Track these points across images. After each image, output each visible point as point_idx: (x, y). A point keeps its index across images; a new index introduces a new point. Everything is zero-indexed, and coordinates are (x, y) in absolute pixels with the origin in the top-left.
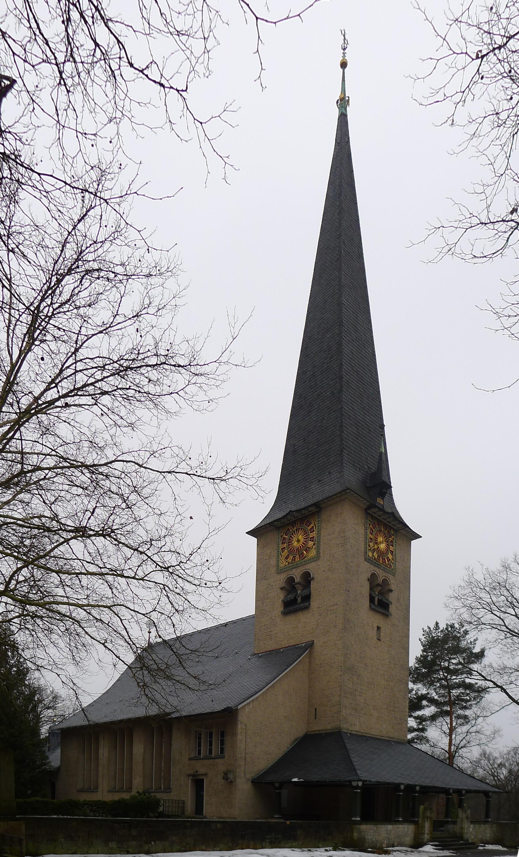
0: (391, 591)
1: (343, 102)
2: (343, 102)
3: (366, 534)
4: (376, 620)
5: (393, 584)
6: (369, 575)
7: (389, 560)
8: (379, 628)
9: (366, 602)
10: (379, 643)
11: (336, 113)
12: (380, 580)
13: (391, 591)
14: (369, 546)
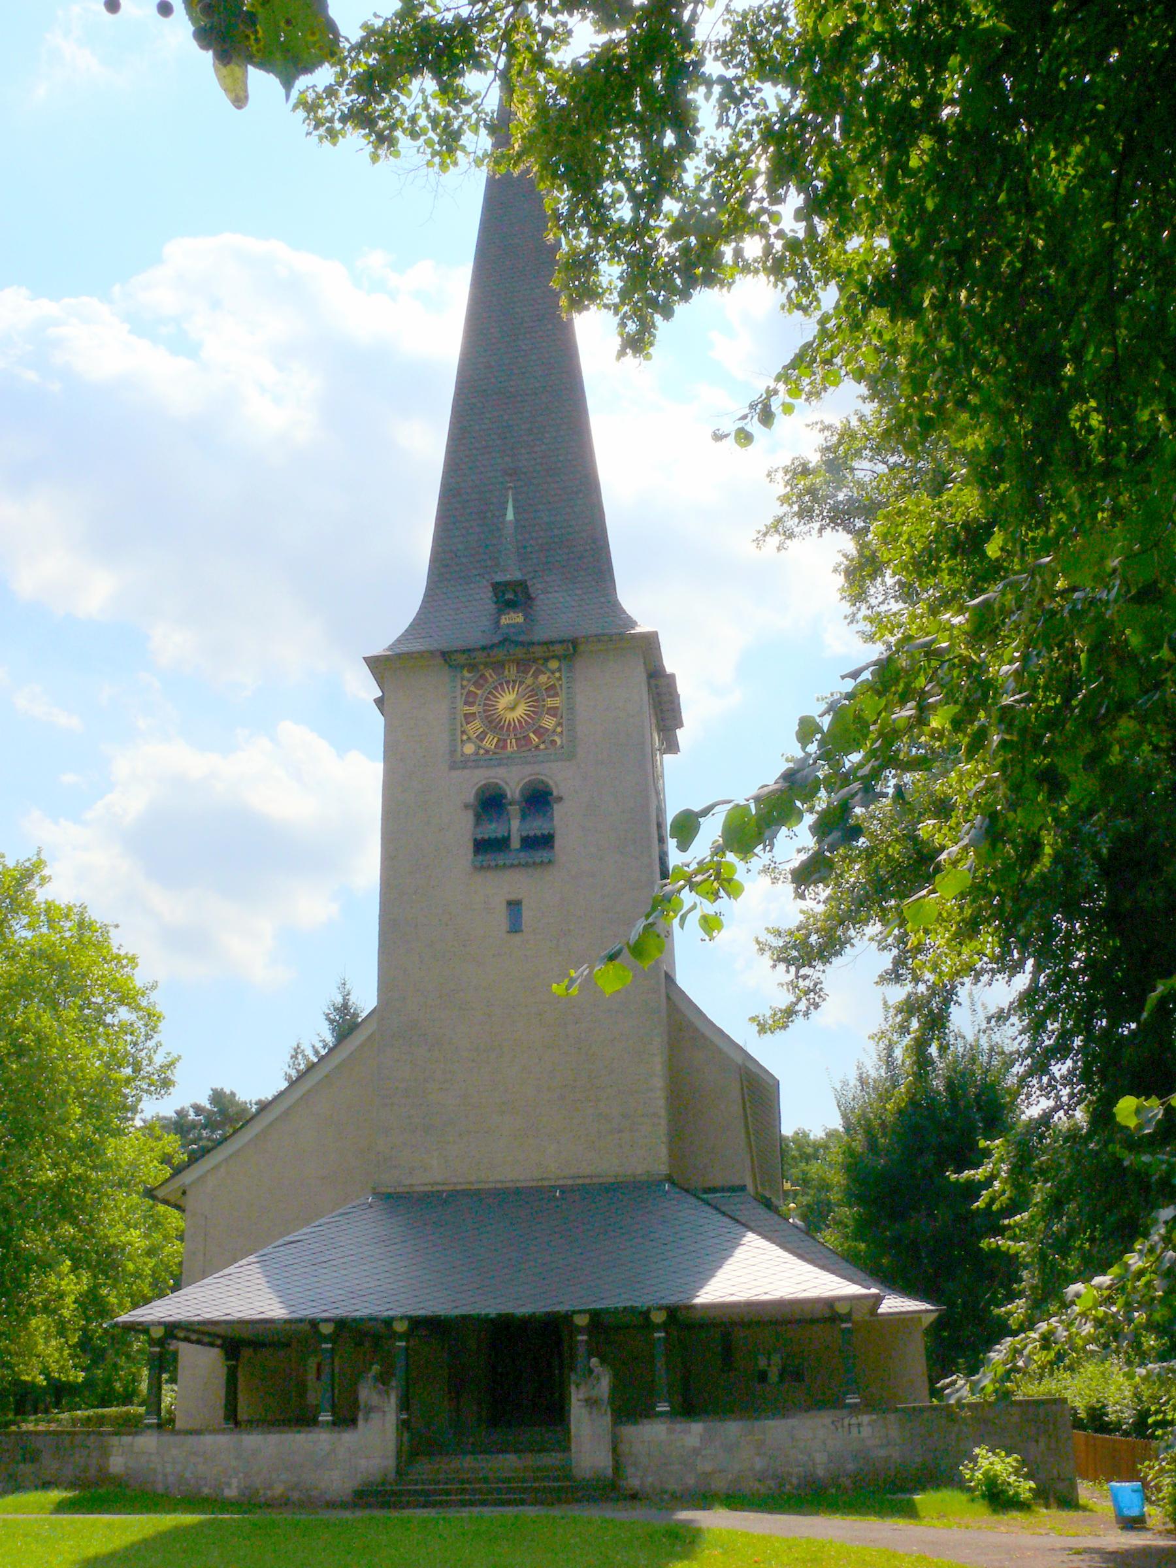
0: (560, 799)
6: (470, 797)
8: (514, 906)
12: (513, 789)
14: (463, 732)
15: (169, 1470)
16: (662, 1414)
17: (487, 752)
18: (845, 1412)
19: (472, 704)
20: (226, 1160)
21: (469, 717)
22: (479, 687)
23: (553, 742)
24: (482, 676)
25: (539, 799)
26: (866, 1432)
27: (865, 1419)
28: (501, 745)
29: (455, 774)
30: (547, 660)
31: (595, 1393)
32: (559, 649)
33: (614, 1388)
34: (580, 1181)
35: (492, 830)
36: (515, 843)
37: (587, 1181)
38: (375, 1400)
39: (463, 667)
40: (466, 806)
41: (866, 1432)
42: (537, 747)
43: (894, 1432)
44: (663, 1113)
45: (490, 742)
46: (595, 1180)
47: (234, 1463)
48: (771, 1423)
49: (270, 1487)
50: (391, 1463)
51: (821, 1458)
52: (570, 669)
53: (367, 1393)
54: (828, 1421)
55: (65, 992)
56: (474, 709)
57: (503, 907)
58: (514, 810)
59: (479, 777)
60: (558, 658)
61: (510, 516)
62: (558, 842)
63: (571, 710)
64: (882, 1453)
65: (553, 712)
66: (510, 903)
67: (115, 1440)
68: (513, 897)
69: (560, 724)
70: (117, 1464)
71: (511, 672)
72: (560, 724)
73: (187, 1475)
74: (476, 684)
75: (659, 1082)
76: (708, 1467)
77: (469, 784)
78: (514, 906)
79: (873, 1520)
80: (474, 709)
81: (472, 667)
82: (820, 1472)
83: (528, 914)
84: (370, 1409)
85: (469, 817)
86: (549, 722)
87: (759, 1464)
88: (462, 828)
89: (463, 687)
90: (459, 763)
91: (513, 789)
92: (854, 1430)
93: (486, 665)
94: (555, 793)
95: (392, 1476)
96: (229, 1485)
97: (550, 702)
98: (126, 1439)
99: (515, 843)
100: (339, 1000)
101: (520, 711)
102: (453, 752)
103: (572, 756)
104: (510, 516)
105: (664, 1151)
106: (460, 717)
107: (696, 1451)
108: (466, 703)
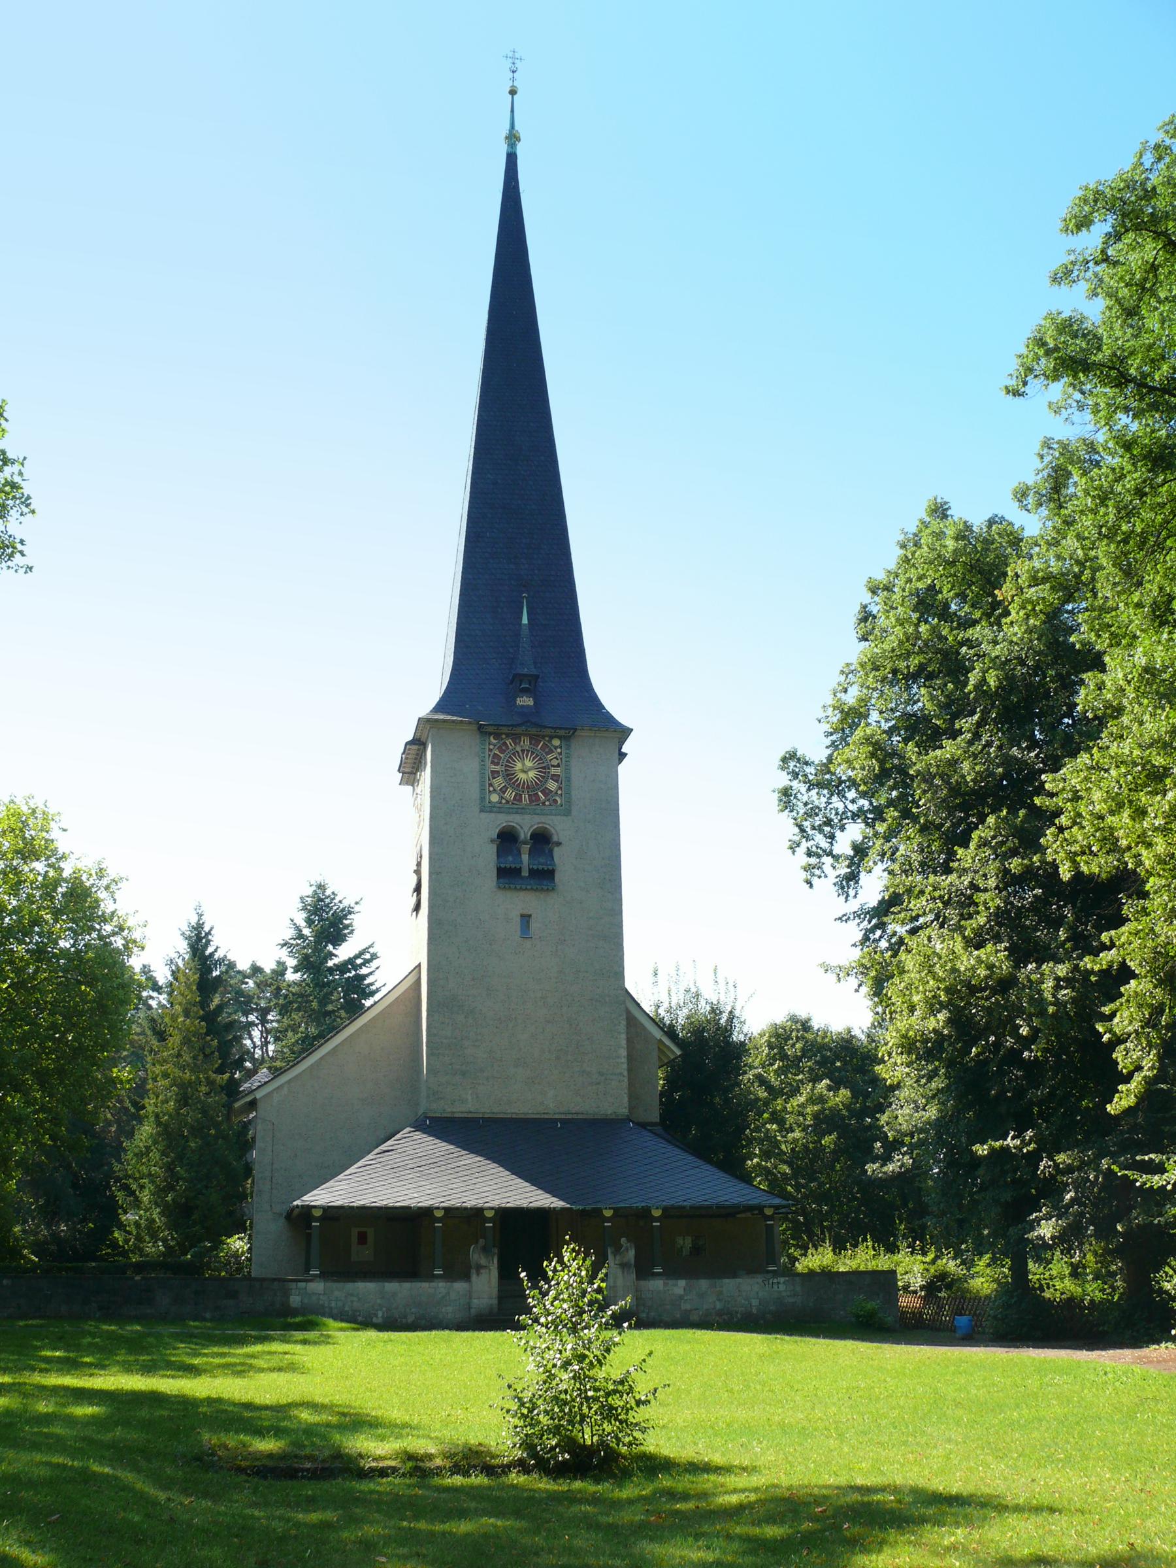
0: (559, 844)
1: (513, 138)
2: (513, 138)
7: (546, 792)
8: (526, 918)
10: (528, 943)
11: (503, 149)
12: (525, 833)
13: (559, 844)
14: (491, 785)
15: (333, 1305)
16: (658, 1274)
17: (508, 802)
18: (770, 1275)
19: (497, 764)
20: (289, 1082)
21: (495, 774)
22: (502, 752)
23: (555, 801)
24: (505, 744)
25: (542, 840)
26: (782, 1287)
27: (782, 1280)
28: (518, 798)
29: (483, 815)
30: (551, 737)
31: (625, 1260)
32: (562, 733)
33: (636, 1257)
34: (570, 1116)
35: (509, 862)
36: (525, 873)
37: (575, 1116)
39: (490, 734)
40: (492, 841)
41: (782, 1287)
42: (544, 803)
43: (798, 1289)
44: (626, 1073)
45: (510, 794)
46: (580, 1116)
47: (379, 1301)
48: (727, 1281)
49: (405, 1317)
50: (495, 1302)
51: (755, 1302)
53: (476, 1256)
54: (760, 1280)
56: (498, 768)
57: (519, 919)
58: (525, 849)
59: (503, 820)
60: (560, 738)
61: (525, 620)
62: (557, 876)
63: (568, 779)
64: (791, 1300)
65: (556, 778)
67: (293, 1285)
68: (525, 912)
69: (560, 788)
70: (295, 1300)
71: (526, 743)
72: (560, 788)
73: (347, 1309)
74: (500, 749)
75: (623, 1052)
76: (688, 1307)
77: (496, 823)
78: (526, 918)
80: (498, 768)
81: (497, 736)
82: (754, 1311)
83: (534, 925)
84: (479, 1268)
86: (552, 785)
87: (719, 1306)
88: (487, 857)
89: (490, 750)
90: (486, 808)
91: (525, 833)
92: (775, 1286)
93: (508, 735)
94: (555, 839)
95: (496, 1310)
96: (376, 1316)
99: (525, 873)
100: (194, 920)
101: (532, 774)
102: (482, 799)
103: (568, 813)
104: (525, 620)
105: (626, 1099)
106: (488, 773)
107: (681, 1297)
108: (492, 762)
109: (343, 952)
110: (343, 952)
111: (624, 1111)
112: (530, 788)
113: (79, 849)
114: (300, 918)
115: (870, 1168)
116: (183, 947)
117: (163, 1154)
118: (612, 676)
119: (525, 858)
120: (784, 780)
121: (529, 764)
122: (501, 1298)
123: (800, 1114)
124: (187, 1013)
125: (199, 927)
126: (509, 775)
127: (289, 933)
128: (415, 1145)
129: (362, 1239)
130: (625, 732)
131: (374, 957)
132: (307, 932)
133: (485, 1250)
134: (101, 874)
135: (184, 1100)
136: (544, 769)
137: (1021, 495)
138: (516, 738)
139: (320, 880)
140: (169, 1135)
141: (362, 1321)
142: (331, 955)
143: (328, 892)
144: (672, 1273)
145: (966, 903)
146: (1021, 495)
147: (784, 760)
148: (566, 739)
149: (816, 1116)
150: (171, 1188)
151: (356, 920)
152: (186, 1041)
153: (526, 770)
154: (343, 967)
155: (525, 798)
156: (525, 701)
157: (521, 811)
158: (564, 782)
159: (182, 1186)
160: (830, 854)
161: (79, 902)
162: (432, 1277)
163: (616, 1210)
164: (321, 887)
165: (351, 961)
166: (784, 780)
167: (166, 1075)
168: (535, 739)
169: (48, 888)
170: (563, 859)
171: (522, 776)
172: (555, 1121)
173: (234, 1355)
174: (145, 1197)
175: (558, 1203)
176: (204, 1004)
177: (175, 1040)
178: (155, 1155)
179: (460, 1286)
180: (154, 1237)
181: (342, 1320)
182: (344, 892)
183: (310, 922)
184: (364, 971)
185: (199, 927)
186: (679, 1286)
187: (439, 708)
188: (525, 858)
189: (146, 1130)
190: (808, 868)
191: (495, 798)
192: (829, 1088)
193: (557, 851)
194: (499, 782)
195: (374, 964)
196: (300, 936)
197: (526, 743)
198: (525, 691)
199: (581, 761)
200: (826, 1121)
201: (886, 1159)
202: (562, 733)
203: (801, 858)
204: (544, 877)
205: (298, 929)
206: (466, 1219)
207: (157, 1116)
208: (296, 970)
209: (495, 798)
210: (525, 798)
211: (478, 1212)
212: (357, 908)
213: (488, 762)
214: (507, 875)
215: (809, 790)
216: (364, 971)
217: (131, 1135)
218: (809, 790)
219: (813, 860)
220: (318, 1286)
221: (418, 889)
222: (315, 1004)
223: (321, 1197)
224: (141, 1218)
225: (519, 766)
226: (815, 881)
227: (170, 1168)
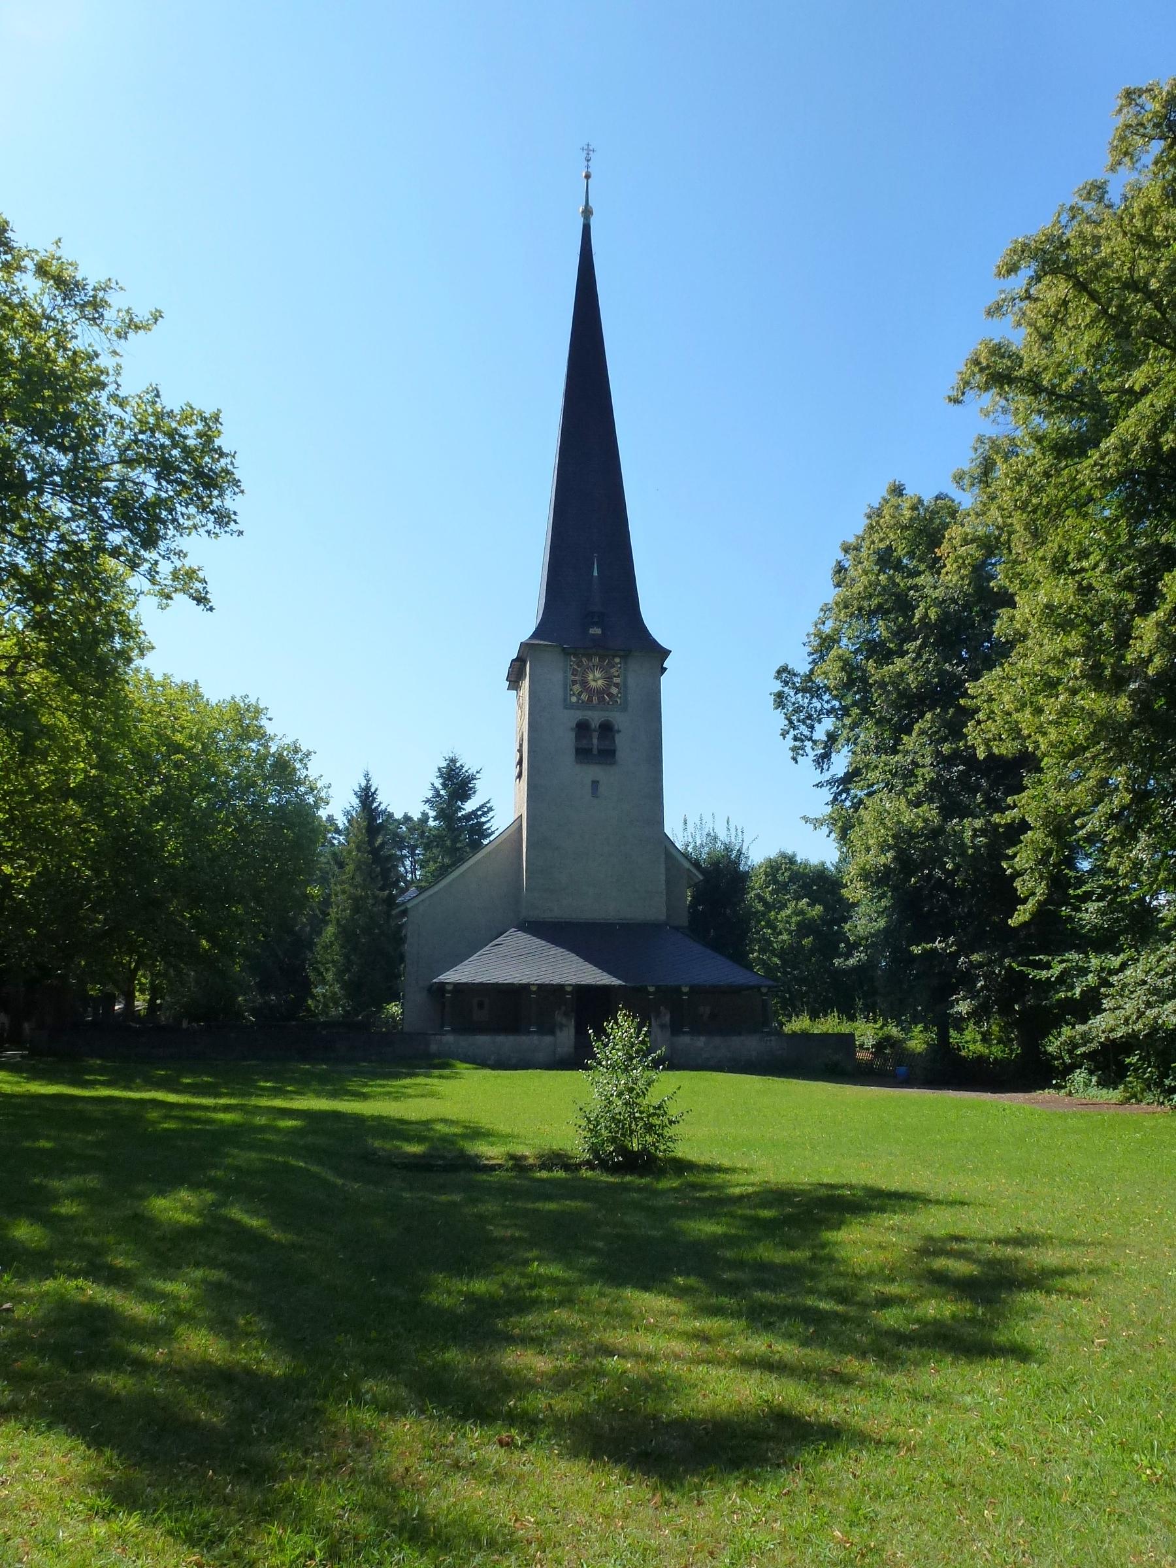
0: (619, 731)
1: (587, 213)
2: (587, 213)
3: (566, 677)
4: (593, 771)
5: (619, 719)
7: (610, 695)
8: (595, 783)
9: (569, 756)
11: (580, 221)
12: (595, 724)
13: (619, 731)
20: (431, 896)
21: (574, 682)
25: (607, 729)
28: (590, 699)
30: (614, 657)
36: (595, 752)
38: (564, 1021)
45: (585, 697)
50: (572, 1050)
52: (626, 663)
53: (559, 1018)
55: (155, 705)
59: (579, 715)
60: (620, 657)
61: (596, 573)
62: (618, 754)
63: (625, 686)
65: (617, 685)
66: (593, 782)
70: (434, 1048)
71: (596, 660)
75: (663, 877)
77: (571, 718)
78: (595, 783)
79: (500, 981)
83: (602, 789)
84: (562, 1026)
85: (572, 735)
86: (614, 691)
88: (567, 740)
90: (568, 706)
91: (595, 724)
93: (583, 655)
94: (616, 727)
97: (615, 680)
98: (438, 1037)
99: (595, 752)
100: (363, 784)
101: (600, 682)
102: (565, 700)
104: (596, 573)
106: (569, 682)
109: (469, 806)
110: (469, 806)
111: (663, 918)
112: (600, 693)
113: (283, 728)
114: (438, 783)
115: (836, 962)
116: (356, 802)
117: (342, 947)
118: (658, 613)
119: (595, 741)
120: (777, 686)
121: (598, 675)
122: (576, 1048)
123: (787, 922)
124: (358, 849)
125: (367, 788)
126: (584, 683)
127: (430, 794)
128: (517, 940)
129: (481, 1005)
130: (665, 653)
131: (490, 809)
132: (442, 792)
133: (566, 1014)
134: (296, 750)
135: (356, 909)
136: (609, 678)
137: (959, 478)
138: (589, 658)
139: (452, 755)
140: (347, 934)
141: (481, 1062)
142: (460, 808)
143: (458, 765)
144: (696, 1031)
145: (909, 775)
146: (959, 478)
147: (779, 672)
148: (625, 657)
149: (798, 924)
150: (348, 970)
151: (478, 784)
152: (358, 868)
153: (596, 679)
154: (468, 817)
155: (595, 699)
156: (596, 631)
157: (593, 708)
158: (622, 687)
159: (355, 969)
160: (810, 739)
161: (283, 770)
162: (529, 1033)
163: (658, 988)
164: (453, 761)
165: (474, 813)
166: (777, 686)
167: (344, 892)
168: (602, 658)
169: (260, 761)
170: (622, 742)
171: (593, 684)
172: (612, 925)
173: (392, 1086)
174: (329, 976)
175: (616, 982)
176: (371, 842)
177: (350, 868)
178: (336, 947)
179: (548, 1039)
180: (336, 1004)
181: (467, 1062)
182: (469, 764)
183: (444, 785)
184: (483, 819)
185: (367, 788)
186: (701, 1041)
187: (535, 635)
188: (595, 741)
189: (331, 930)
190: (794, 749)
191: (574, 699)
192: (808, 905)
193: (618, 738)
194: (577, 688)
195: (491, 814)
196: (438, 795)
197: (596, 660)
198: (594, 624)
199: (635, 675)
200: (806, 927)
201: (849, 955)
202: (622, 653)
203: (789, 742)
204: (607, 755)
205: (437, 790)
206: (552, 993)
207: (338, 920)
208: (435, 819)
209: (574, 699)
210: (595, 699)
211: (561, 987)
212: (478, 776)
213: (569, 674)
214: (583, 754)
215: (796, 694)
216: (483, 819)
217: (319, 933)
218: (796, 694)
219: (798, 744)
220: (450, 1038)
221: (520, 763)
222: (448, 843)
223: (453, 976)
224: (327, 991)
225: (591, 677)
226: (799, 758)
227: (346, 957)
